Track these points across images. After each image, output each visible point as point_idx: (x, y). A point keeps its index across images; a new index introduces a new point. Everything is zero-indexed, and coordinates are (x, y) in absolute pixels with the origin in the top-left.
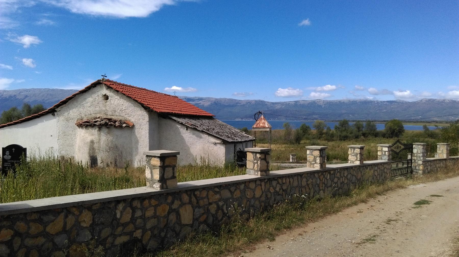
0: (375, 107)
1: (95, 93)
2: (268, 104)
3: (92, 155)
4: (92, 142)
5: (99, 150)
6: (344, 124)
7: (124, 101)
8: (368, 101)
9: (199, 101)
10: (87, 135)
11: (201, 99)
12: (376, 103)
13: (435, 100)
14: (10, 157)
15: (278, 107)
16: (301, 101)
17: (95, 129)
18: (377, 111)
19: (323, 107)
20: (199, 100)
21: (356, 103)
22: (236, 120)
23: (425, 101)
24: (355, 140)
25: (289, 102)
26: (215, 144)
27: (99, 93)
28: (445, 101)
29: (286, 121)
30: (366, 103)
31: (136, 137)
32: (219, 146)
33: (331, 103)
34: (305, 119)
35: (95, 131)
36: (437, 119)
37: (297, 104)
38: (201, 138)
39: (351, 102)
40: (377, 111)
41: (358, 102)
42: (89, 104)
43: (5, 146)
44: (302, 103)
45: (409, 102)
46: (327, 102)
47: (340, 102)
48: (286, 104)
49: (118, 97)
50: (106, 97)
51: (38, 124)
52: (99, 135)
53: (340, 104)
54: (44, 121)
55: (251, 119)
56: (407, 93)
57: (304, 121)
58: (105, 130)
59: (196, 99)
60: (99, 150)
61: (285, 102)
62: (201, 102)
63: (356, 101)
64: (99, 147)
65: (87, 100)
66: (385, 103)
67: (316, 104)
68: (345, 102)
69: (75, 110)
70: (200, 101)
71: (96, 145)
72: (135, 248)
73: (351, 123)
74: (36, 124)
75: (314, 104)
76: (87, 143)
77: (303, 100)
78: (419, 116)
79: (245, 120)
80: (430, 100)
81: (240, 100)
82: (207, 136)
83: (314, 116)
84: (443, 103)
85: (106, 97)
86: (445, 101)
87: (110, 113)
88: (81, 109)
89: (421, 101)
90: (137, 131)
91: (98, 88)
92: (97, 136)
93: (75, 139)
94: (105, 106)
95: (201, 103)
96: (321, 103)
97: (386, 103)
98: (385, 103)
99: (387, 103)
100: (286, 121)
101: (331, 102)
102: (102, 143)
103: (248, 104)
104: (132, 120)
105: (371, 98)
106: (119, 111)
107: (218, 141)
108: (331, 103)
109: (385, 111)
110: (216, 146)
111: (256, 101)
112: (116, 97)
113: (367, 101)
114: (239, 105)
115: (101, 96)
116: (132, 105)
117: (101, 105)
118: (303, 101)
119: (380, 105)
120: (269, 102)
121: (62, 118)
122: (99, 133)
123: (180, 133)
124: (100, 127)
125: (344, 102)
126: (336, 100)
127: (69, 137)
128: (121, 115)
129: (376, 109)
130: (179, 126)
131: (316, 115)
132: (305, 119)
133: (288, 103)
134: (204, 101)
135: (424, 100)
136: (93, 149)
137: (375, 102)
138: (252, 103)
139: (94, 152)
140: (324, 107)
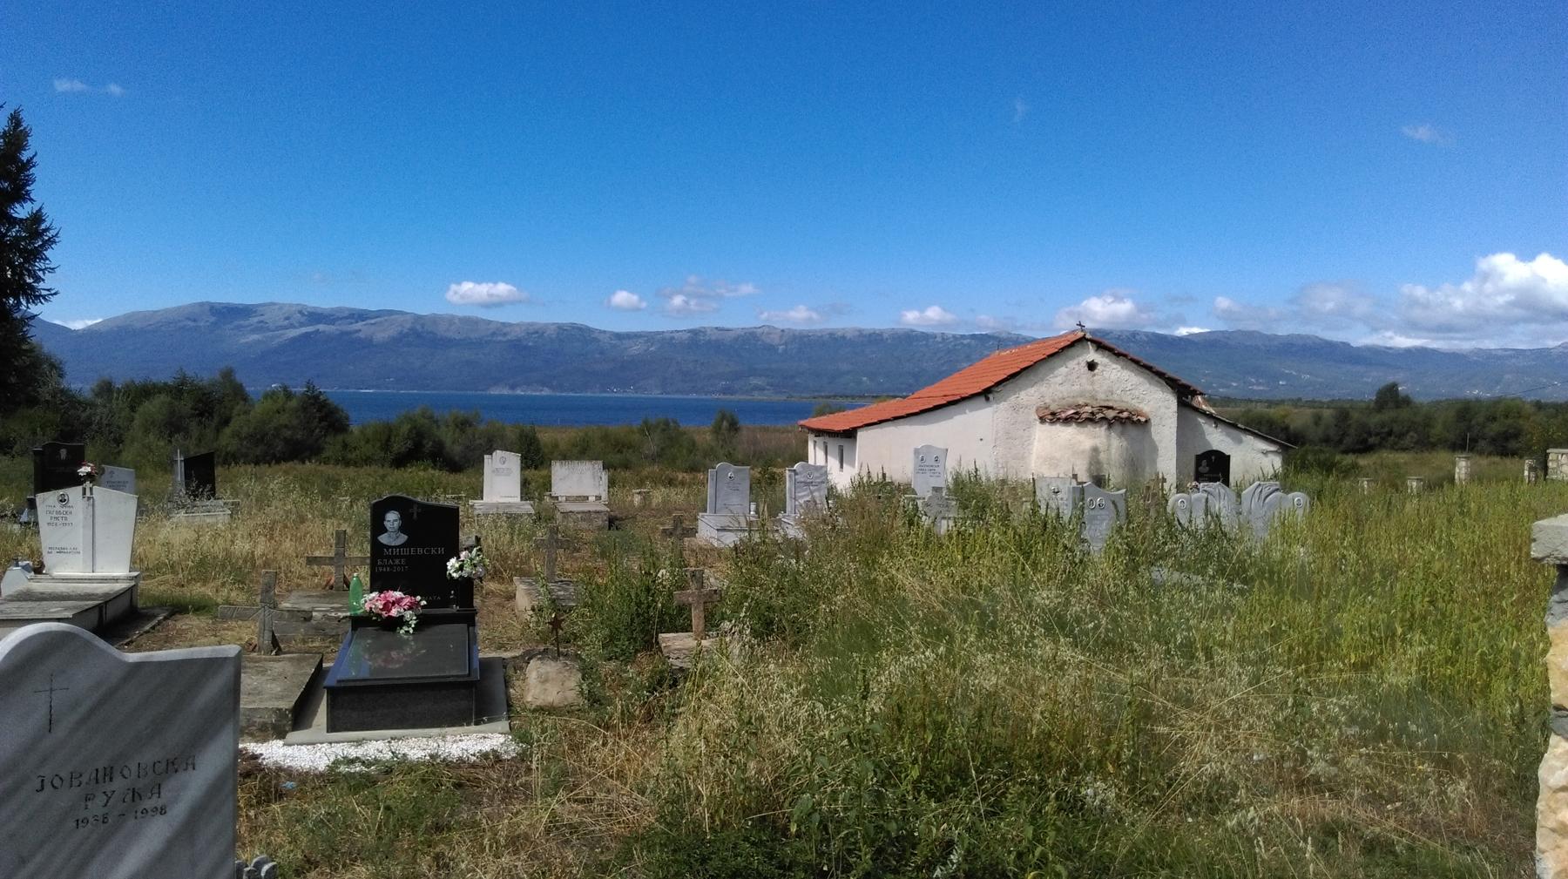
0: (935, 353)
1: (1072, 358)
2: (601, 337)
3: (1095, 474)
4: (1095, 450)
5: (1109, 464)
7: (1129, 373)
8: (916, 335)
9: (352, 323)
11: (361, 316)
12: (939, 339)
13: (1108, 334)
14: (1207, 468)
15: (636, 349)
16: (712, 329)
17: (1101, 426)
18: (943, 365)
20: (353, 321)
21: (882, 340)
22: (492, 393)
25: (672, 332)
26: (1265, 453)
27: (1081, 359)
31: (1152, 442)
32: (1271, 456)
34: (725, 391)
35: (1101, 431)
39: (865, 336)
40: (943, 365)
41: (885, 336)
42: (1059, 378)
43: (1199, 453)
44: (713, 338)
46: (794, 335)
49: (1119, 367)
50: (1092, 366)
51: (955, 417)
52: (1108, 437)
54: (967, 411)
55: (545, 388)
57: (722, 396)
58: (1118, 427)
59: (341, 315)
60: (1109, 464)
61: (658, 333)
62: (359, 325)
63: (880, 335)
65: (1056, 372)
66: (965, 342)
67: (760, 343)
68: (849, 336)
69: (1032, 390)
70: (357, 322)
71: (1102, 456)
72: (1150, 629)
76: (1083, 452)
77: (717, 328)
79: (523, 393)
81: (503, 324)
82: (1252, 438)
83: (755, 381)
84: (1132, 344)
85: (1092, 366)
86: (1138, 337)
93: (1029, 444)
94: (1092, 383)
95: (360, 330)
96: (775, 340)
97: (968, 341)
100: (665, 396)
101: (805, 336)
102: (1113, 451)
103: (534, 336)
104: (1146, 408)
106: (1119, 392)
107: (1273, 448)
110: (1267, 457)
111: (560, 328)
112: (1114, 366)
113: (914, 333)
114: (500, 338)
115: (1084, 364)
116: (1146, 381)
118: (715, 331)
119: (950, 346)
120: (605, 332)
121: (1003, 405)
122: (1108, 433)
123: (1203, 433)
124: (1109, 423)
125: (843, 337)
126: (821, 331)
127: (1017, 442)
128: (1124, 399)
130: (1201, 420)
131: (760, 376)
132: (725, 391)
133: (668, 336)
134: (373, 321)
136: (1098, 462)
137: (936, 337)
138: (545, 335)
139: (1099, 469)
140: (785, 351)
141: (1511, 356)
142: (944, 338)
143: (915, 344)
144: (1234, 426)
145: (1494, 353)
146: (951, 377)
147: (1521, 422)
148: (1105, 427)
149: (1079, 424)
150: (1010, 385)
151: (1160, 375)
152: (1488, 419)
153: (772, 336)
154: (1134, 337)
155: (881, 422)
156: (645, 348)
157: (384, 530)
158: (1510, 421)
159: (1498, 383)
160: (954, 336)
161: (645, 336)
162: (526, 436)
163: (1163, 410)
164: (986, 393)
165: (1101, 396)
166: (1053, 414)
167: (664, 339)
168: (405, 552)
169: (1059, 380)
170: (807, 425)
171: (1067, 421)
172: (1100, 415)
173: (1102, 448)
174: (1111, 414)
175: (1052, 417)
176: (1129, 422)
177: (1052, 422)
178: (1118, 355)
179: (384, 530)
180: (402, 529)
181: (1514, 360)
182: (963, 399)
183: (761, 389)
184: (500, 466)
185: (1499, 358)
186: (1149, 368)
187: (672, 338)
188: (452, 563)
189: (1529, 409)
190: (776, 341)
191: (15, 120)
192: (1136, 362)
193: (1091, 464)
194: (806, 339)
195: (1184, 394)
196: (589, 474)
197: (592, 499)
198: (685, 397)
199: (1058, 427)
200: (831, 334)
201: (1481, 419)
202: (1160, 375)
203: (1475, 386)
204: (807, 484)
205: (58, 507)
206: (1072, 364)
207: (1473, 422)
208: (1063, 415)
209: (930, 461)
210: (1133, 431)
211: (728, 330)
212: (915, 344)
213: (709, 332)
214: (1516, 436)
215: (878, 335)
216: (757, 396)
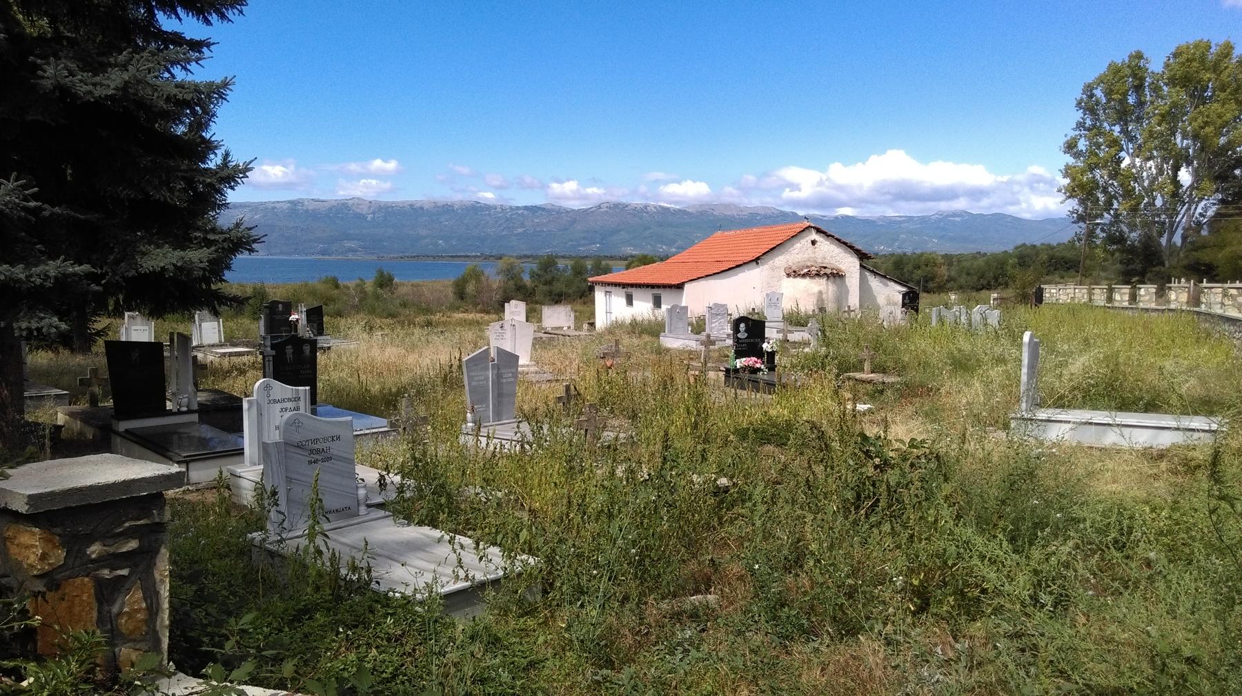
0: (496, 221)
4: (820, 292)
6: (548, 264)
8: (481, 207)
12: (499, 210)
16: (308, 200)
18: (503, 230)
21: (453, 210)
24: (582, 300)
25: (274, 203)
30: (477, 210)
31: (847, 287)
33: (390, 209)
34: (323, 253)
35: (823, 281)
37: (298, 210)
38: (887, 286)
40: (503, 230)
44: (310, 208)
50: (814, 243)
52: (827, 285)
53: (413, 212)
56: (570, 187)
57: (321, 257)
58: (832, 278)
61: (261, 204)
63: (452, 206)
66: (520, 212)
69: (781, 258)
71: (824, 296)
73: (561, 264)
75: (342, 213)
76: (814, 294)
80: (616, 206)
83: (348, 244)
85: (814, 243)
88: (787, 257)
89: (599, 207)
92: (825, 286)
98: (520, 212)
102: (830, 293)
104: (843, 267)
105: (488, 196)
109: (520, 230)
115: (810, 241)
121: (766, 267)
125: (422, 208)
126: (403, 202)
129: (500, 226)
132: (323, 253)
133: (270, 206)
136: (822, 300)
139: (823, 304)
142: (503, 209)
144: (885, 277)
145: (893, 219)
146: (687, 251)
147: (936, 269)
149: (811, 277)
151: (851, 247)
152: (915, 268)
153: (361, 206)
154: (646, 209)
155: (699, 278)
158: (929, 269)
160: (511, 207)
161: (249, 206)
164: (757, 260)
165: (820, 261)
166: (794, 272)
167: (266, 208)
168: (747, 341)
169: (796, 251)
170: (605, 280)
171: (804, 276)
173: (824, 291)
174: (828, 271)
175: (793, 273)
176: (836, 276)
177: (795, 277)
178: (828, 236)
180: (746, 331)
183: (354, 251)
189: (940, 260)
191: (225, 84)
192: (839, 240)
193: (818, 301)
194: (390, 209)
195: (862, 256)
196: (563, 313)
197: (565, 328)
198: (288, 258)
199: (799, 280)
200: (411, 205)
202: (851, 247)
203: (881, 244)
204: (717, 315)
205: (500, 330)
206: (803, 241)
207: (905, 270)
208: (802, 273)
210: (838, 279)
213: (306, 203)
214: (932, 279)
215: (450, 206)
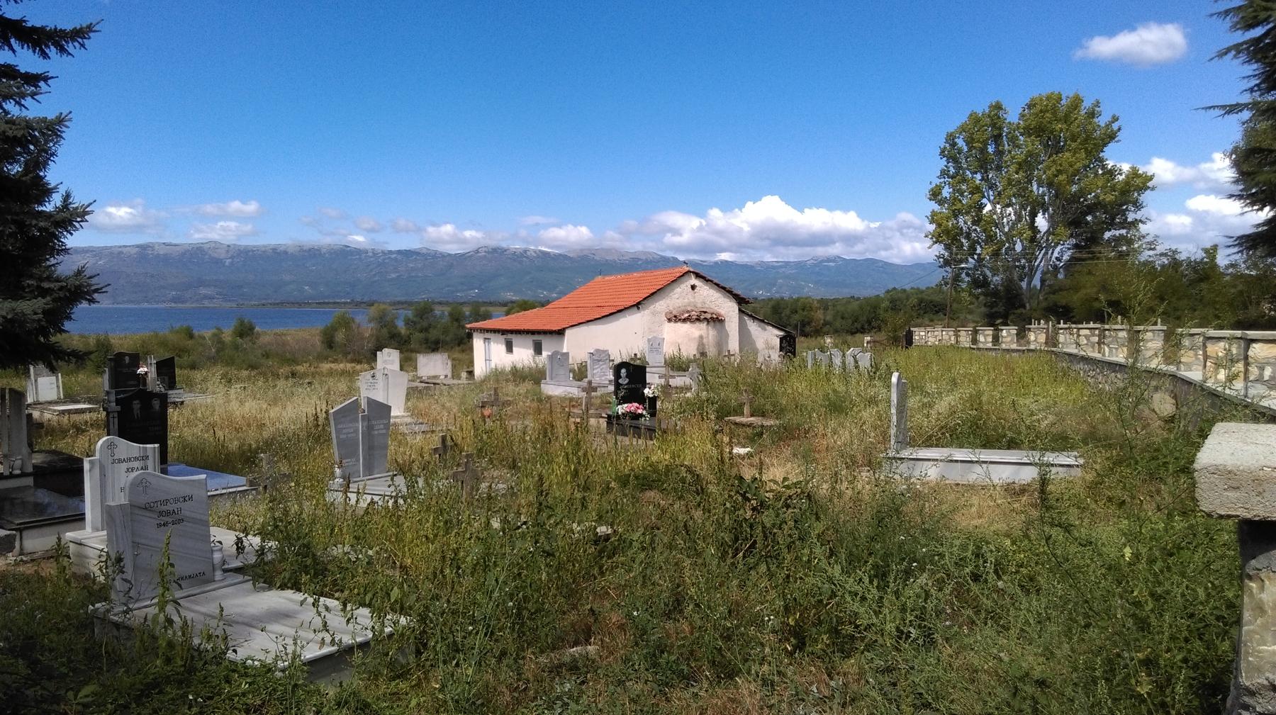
1: (683, 283)
4: (701, 337)
6: (424, 311)
10: (694, 330)
12: (371, 254)
13: (506, 251)
16: (159, 244)
18: (375, 275)
19: (227, 264)
21: (320, 254)
23: (485, 252)
25: (120, 247)
28: (528, 253)
29: (115, 306)
34: (175, 300)
35: (703, 325)
36: (513, 296)
38: (765, 330)
45: (449, 255)
47: (274, 250)
48: (111, 253)
50: (693, 287)
52: (708, 329)
53: (277, 256)
57: (173, 305)
58: (712, 323)
61: (106, 248)
63: (319, 250)
64: (708, 342)
65: (675, 291)
67: (207, 257)
68: (290, 250)
69: (662, 302)
71: (705, 340)
74: (618, 320)
75: (197, 256)
78: (474, 289)
83: (203, 291)
85: (693, 287)
86: (528, 253)
87: (699, 305)
89: (477, 251)
90: (727, 324)
91: (686, 277)
92: (705, 331)
94: (694, 297)
96: (222, 254)
99: (399, 257)
100: (115, 306)
104: (722, 312)
108: (251, 253)
109: (393, 276)
117: (690, 297)
118: (163, 246)
125: (286, 252)
135: (484, 249)
136: (703, 344)
140: (232, 263)
141: (781, 267)
142: (375, 253)
143: (349, 257)
145: (771, 264)
148: (706, 323)
150: (650, 300)
156: (94, 262)
157: (621, 377)
158: (805, 313)
159: (774, 285)
162: (103, 345)
163: (731, 313)
164: (638, 305)
166: (675, 316)
169: (677, 296)
171: (685, 320)
172: (702, 317)
173: (704, 335)
174: (708, 316)
175: (674, 318)
176: (716, 320)
177: (676, 322)
179: (621, 377)
180: (627, 377)
181: (783, 270)
182: (626, 309)
183: (211, 298)
184: (387, 358)
185: (774, 267)
186: (724, 288)
187: (121, 253)
188: (646, 391)
189: (816, 304)
190: (223, 256)
192: (717, 285)
195: (740, 301)
197: (442, 377)
199: (679, 324)
201: (787, 312)
205: (371, 380)
206: (683, 286)
208: (683, 317)
209: (655, 345)
211: (176, 245)
212: (349, 257)
216: (206, 303)
